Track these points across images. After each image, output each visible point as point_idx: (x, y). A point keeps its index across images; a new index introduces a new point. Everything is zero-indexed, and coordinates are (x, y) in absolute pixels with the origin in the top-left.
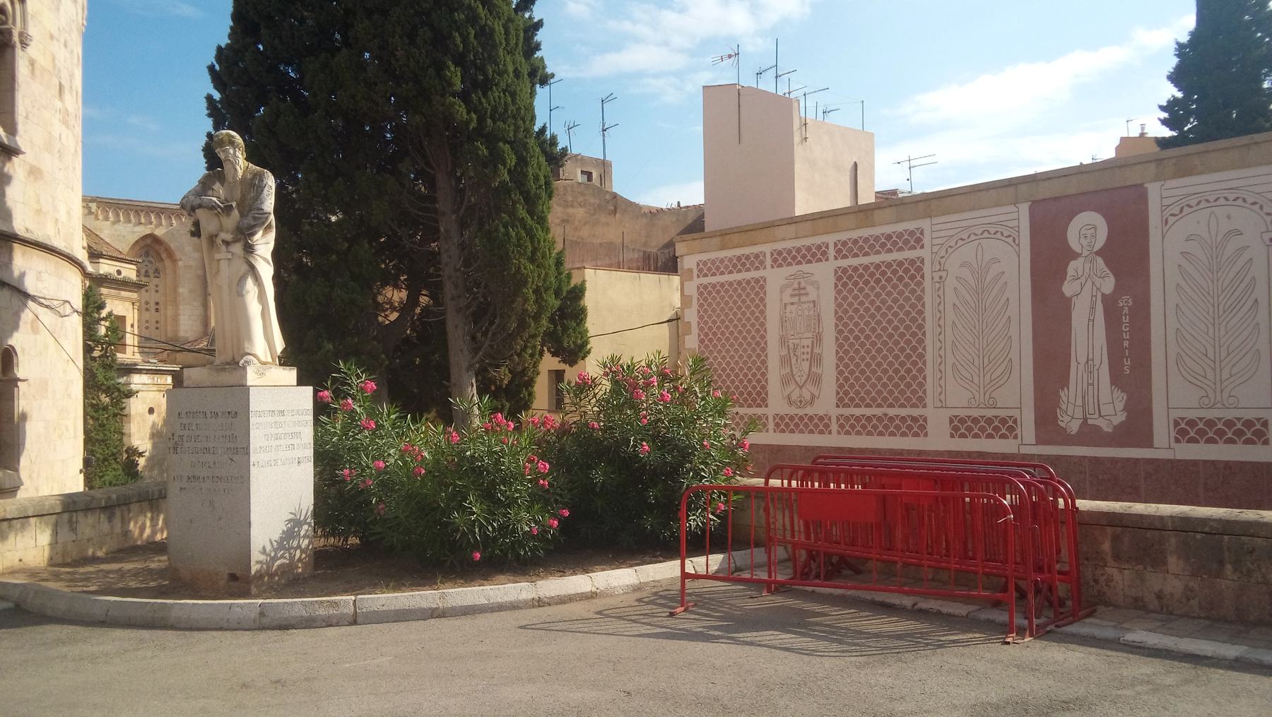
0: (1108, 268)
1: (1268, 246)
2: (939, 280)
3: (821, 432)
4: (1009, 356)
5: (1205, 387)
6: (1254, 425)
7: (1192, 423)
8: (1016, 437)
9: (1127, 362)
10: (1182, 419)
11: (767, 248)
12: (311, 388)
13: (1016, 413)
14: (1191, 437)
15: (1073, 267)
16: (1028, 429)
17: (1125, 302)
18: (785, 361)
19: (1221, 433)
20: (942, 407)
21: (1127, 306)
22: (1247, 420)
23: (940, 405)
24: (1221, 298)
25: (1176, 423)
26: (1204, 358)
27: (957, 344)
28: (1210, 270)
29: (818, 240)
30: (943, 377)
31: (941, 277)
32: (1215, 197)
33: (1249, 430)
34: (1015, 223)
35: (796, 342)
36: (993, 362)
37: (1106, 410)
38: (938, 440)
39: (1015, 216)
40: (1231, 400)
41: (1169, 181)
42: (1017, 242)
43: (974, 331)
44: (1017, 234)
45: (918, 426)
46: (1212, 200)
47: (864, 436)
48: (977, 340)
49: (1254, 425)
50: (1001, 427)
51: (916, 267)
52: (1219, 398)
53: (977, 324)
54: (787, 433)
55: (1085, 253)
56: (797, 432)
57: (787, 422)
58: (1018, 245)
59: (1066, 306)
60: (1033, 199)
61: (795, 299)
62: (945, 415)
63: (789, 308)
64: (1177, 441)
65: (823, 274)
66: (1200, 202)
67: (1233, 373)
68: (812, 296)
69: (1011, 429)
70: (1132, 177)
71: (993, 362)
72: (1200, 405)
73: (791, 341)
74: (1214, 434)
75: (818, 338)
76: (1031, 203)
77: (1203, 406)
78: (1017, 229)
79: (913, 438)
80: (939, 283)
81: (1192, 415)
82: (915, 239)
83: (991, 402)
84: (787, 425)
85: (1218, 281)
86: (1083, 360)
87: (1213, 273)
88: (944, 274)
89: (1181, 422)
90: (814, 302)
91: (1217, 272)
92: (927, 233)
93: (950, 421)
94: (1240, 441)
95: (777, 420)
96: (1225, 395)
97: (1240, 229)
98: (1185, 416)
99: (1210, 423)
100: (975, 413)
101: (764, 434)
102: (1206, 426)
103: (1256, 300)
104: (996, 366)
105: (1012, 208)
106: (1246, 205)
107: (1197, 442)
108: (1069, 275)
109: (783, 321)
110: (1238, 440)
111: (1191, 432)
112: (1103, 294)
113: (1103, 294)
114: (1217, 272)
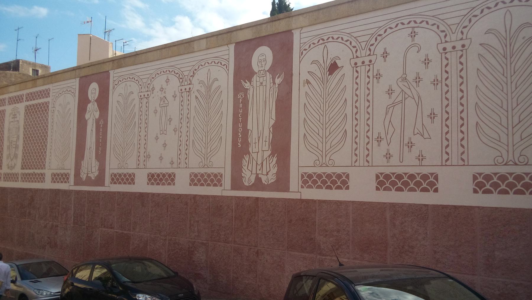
0: (98, 108)
1: (442, 53)
2: (462, 49)
3: (339, 188)
4: (134, 142)
5: (499, 148)
6: (524, 179)
7: (488, 177)
8: (221, 185)
9: (240, 140)
10: (480, 174)
11: (6, 96)
12: (248, 128)
13: (222, 171)
14: (487, 189)
15: (90, 106)
16: (227, 181)
17: (101, 122)
18: (9, 148)
19: (418, 184)
20: (186, 167)
21: (102, 124)
22: (518, 175)
23: (462, 163)
24: (513, 78)
25: (302, 176)
26: (500, 126)
27: (196, 129)
28: (504, 57)
29: (19, 93)
30: (354, 138)
31: (148, 95)
32: (408, 21)
33: (519, 183)
34: (226, 57)
35: (12, 139)
36: (212, 140)
37: (94, 170)
38: (48, 185)
39: (227, 52)
40: (330, 162)
41: (116, 70)
42: (228, 69)
43: (122, 129)
44: (228, 63)
45: (41, 178)
46: (418, 22)
47: (127, 185)
48: (321, 117)
49: (524, 179)
50: (386, 181)
51: (47, 104)
52: (324, 161)
53: (322, 105)
54: (205, 186)
55: (92, 101)
56: (344, 188)
57: (64, 177)
58: (228, 70)
59: (86, 122)
60: (236, 42)
61: (13, 120)
62: (188, 172)
63: (12, 123)
64: (302, 187)
65: (21, 107)
66: (397, 25)
67: (523, 137)
68: (18, 119)
69: (432, 184)
70: (106, 67)
71: (212, 140)
72: (495, 163)
73: (11, 139)
74: (506, 186)
75: (18, 138)
76: (79, 78)
77: (497, 164)
78: (228, 60)
79: (472, 189)
80: (462, 51)
81: (487, 171)
82: (46, 93)
83: (330, 163)
84: (199, 180)
85: (511, 64)
86: (89, 148)
87: (506, 59)
88: (467, 42)
89: (494, 176)
90: (18, 121)
91: (511, 58)
92: (51, 90)
93: (148, 176)
94: (496, 191)
95: (193, 177)
96: (517, 155)
97: (133, 92)
98: (200, 172)
99: (503, 178)
100: (503, 170)
101: (17, 183)
102: (516, 180)
103: (346, 100)
104: (214, 142)
105: (225, 48)
106: (383, 36)
107: (508, 193)
108: (87, 110)
109: (9, 130)
110: (392, 188)
111: (518, 185)
112: (96, 119)
113: (96, 119)
114: (511, 58)
